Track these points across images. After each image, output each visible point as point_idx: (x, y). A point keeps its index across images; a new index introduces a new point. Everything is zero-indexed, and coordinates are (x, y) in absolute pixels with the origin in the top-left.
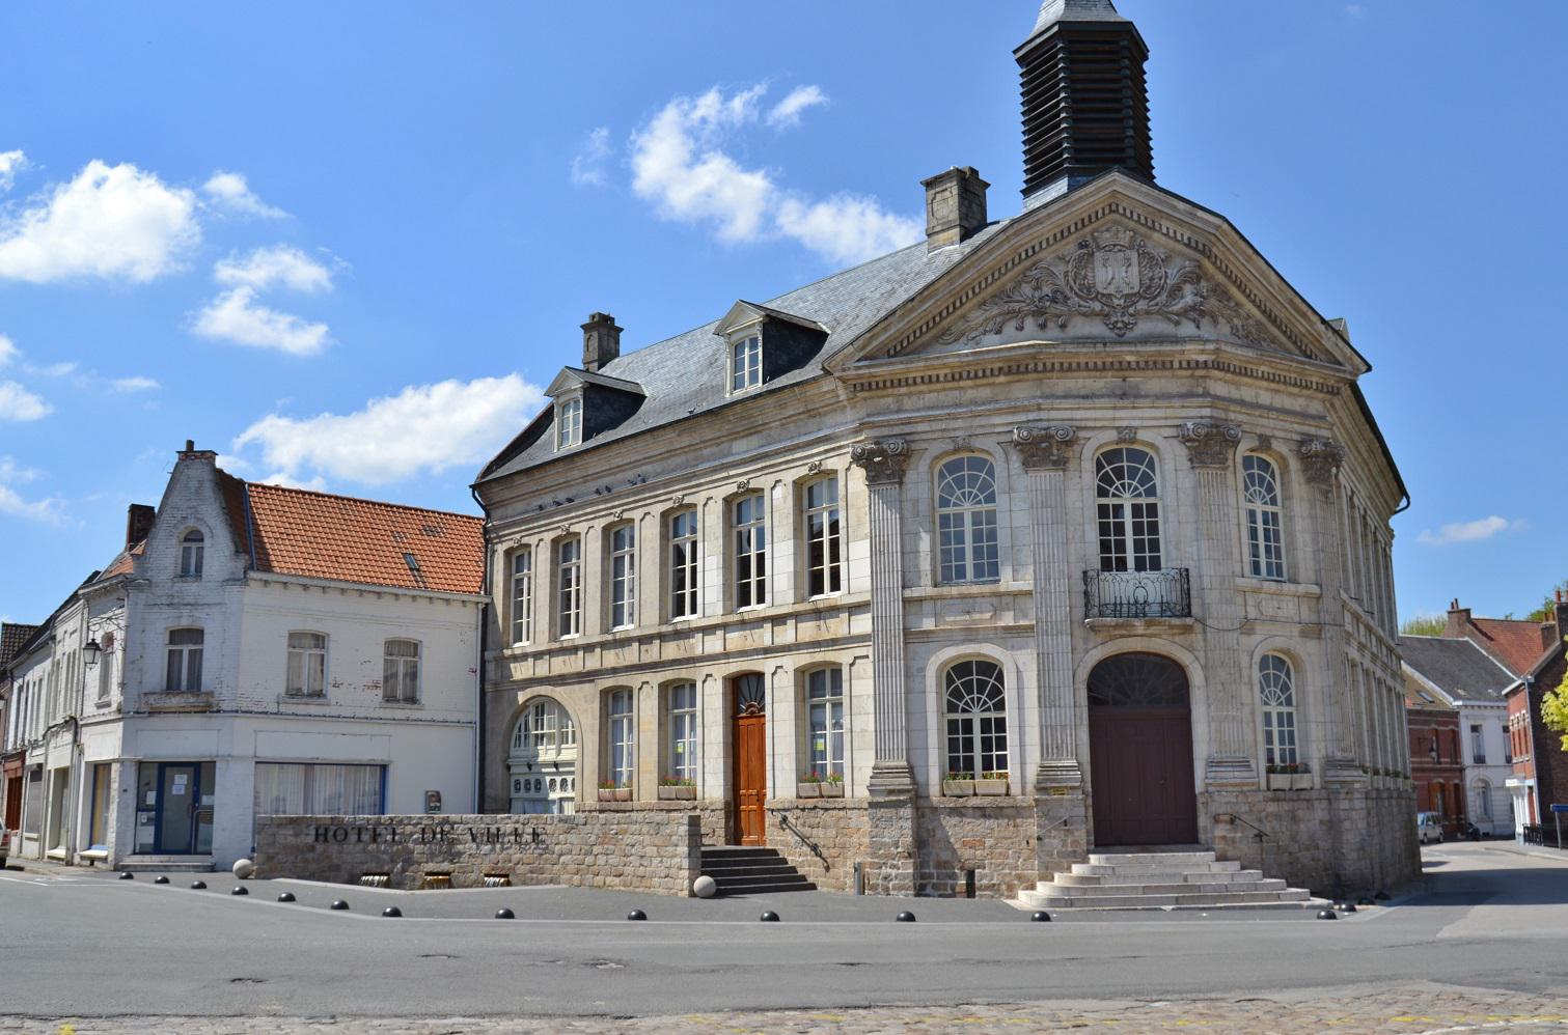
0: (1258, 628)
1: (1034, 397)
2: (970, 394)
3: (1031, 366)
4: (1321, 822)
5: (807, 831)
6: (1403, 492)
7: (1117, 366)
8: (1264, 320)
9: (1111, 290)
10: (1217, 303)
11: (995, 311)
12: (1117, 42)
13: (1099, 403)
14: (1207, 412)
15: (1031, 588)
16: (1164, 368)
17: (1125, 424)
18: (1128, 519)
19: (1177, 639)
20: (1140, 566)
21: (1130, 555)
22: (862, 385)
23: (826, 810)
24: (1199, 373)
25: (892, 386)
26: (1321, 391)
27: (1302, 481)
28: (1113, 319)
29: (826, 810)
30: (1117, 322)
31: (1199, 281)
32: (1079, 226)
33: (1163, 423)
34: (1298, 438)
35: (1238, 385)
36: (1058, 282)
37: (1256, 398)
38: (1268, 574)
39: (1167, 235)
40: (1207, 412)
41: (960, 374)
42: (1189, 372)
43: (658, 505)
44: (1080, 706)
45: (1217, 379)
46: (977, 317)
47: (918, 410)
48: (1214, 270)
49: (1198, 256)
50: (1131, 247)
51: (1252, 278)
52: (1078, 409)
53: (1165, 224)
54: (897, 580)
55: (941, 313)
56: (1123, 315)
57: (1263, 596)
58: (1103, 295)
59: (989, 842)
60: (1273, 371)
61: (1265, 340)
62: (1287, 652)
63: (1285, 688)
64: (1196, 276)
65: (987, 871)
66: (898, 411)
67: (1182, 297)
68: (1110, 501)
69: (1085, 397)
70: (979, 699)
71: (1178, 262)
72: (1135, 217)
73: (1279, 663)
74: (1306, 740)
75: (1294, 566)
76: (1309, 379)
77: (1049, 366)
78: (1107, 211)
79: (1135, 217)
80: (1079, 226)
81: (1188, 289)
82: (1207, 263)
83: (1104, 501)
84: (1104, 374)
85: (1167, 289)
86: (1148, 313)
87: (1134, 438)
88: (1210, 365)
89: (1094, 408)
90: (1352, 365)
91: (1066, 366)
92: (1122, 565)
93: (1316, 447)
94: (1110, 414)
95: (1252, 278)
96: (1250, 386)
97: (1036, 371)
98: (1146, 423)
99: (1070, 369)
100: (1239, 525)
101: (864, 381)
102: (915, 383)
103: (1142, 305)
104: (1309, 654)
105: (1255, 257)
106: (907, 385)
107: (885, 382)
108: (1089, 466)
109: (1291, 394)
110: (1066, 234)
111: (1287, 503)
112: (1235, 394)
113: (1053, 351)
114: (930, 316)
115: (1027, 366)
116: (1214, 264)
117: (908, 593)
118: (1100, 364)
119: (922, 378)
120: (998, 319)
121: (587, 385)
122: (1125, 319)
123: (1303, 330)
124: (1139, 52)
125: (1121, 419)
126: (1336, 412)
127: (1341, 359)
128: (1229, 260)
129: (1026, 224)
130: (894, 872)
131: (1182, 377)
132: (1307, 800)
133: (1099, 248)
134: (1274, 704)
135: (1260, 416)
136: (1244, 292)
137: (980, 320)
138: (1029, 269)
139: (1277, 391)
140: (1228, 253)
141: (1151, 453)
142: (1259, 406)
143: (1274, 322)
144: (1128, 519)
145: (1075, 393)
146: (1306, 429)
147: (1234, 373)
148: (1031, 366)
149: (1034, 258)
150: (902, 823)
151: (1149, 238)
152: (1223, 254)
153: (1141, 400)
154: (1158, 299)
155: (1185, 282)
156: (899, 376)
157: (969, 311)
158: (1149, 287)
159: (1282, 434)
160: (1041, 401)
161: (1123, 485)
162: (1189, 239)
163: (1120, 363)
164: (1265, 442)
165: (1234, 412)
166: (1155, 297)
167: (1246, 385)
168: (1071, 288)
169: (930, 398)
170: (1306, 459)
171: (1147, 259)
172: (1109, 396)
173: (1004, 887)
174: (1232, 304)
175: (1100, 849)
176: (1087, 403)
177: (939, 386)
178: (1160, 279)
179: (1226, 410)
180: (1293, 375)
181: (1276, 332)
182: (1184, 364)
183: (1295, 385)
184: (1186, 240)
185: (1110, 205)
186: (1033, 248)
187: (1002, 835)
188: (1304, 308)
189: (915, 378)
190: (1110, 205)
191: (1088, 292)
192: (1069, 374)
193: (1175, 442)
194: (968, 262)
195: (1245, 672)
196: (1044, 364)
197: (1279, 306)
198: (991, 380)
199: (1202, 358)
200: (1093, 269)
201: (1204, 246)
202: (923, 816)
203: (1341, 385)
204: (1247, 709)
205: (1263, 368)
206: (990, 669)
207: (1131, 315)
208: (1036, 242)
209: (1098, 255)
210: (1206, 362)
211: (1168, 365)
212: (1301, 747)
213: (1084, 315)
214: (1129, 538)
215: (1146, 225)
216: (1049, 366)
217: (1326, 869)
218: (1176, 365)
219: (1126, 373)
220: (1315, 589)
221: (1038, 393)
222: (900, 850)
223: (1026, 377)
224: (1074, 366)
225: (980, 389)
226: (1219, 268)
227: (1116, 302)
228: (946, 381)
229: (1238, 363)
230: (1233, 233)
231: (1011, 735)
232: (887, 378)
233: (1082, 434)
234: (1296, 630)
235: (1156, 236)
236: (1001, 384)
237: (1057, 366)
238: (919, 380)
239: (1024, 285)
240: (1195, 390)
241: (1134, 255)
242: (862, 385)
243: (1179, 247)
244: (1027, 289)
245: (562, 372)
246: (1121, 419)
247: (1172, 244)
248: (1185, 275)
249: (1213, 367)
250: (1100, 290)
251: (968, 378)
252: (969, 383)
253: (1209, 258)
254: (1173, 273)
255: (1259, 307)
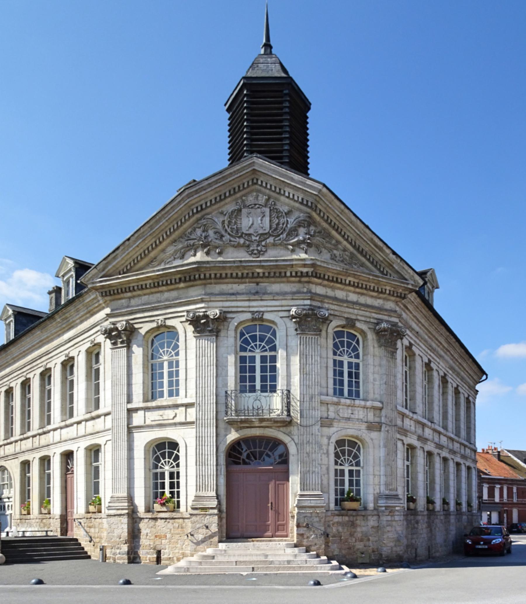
0: (335, 424)
1: (200, 295)
2: (166, 295)
3: (197, 276)
4: (373, 527)
5: (88, 529)
6: (483, 373)
7: (250, 275)
8: (355, 252)
9: (251, 231)
10: (321, 240)
11: (180, 246)
12: (282, 91)
13: (239, 297)
14: (308, 302)
15: (194, 401)
16: (280, 276)
17: (255, 309)
18: (258, 364)
19: (281, 429)
20: (264, 389)
21: (258, 384)
22: (106, 292)
23: (95, 519)
24: (304, 279)
25: (122, 292)
26: (393, 295)
27: (376, 345)
28: (251, 248)
29: (95, 519)
30: (253, 250)
31: (309, 226)
32: (232, 192)
33: (280, 308)
34: (375, 321)
35: (333, 288)
36: (218, 227)
37: (346, 297)
38: (349, 396)
39: (288, 197)
40: (308, 302)
41: (158, 283)
42: (298, 279)
43: (39, 369)
44: (221, 465)
45: (317, 284)
46: (171, 250)
47: (138, 306)
48: (325, 221)
49: (309, 210)
50: (266, 206)
51: (346, 225)
52: (227, 301)
53: (287, 190)
54: (125, 398)
55: (148, 248)
56: (258, 245)
57: (340, 407)
58: (246, 234)
59: (168, 536)
60: (356, 281)
61: (355, 264)
62: (357, 438)
63: (356, 457)
64: (309, 222)
65: (167, 551)
66: (128, 307)
67: (297, 235)
68: (248, 354)
69: (233, 294)
70: (169, 462)
71: (296, 214)
72: (269, 187)
73: (353, 444)
74: (366, 485)
75: (366, 392)
76: (384, 287)
77: (208, 276)
78: (250, 183)
79: (269, 187)
80: (232, 192)
81: (302, 231)
82: (314, 214)
83: (243, 354)
84: (243, 280)
85: (287, 230)
86: (274, 245)
87: (262, 317)
88: (310, 274)
89: (236, 300)
90: (415, 281)
91: (218, 275)
92: (253, 389)
93: (384, 325)
94: (247, 304)
95: (346, 225)
96: (342, 290)
97: (200, 279)
98: (269, 309)
99: (221, 277)
100: (327, 367)
101: (106, 290)
102: (134, 290)
103: (271, 240)
104: (372, 439)
105: (346, 211)
106: (130, 291)
107: (118, 290)
108: (231, 333)
109: (372, 297)
110: (223, 197)
111: (365, 357)
112: (330, 293)
113: (208, 265)
114: (142, 251)
115: (195, 276)
116: (319, 215)
117: (130, 406)
118: (240, 274)
119: (138, 286)
120: (182, 251)
121: (16, 313)
122: (259, 248)
123: (381, 259)
124: (301, 105)
125: (253, 307)
126: (411, 313)
127: (406, 277)
128: (329, 213)
129: (194, 189)
130: (118, 551)
131: (294, 282)
132: (364, 516)
133: (245, 206)
134: (347, 465)
135: (347, 307)
136: (340, 233)
137: (172, 252)
138: (200, 219)
139: (362, 294)
140: (328, 208)
141: (274, 326)
142: (347, 301)
143: (361, 253)
144: (258, 364)
145: (226, 292)
146: (380, 316)
147: (328, 280)
148: (197, 276)
149: (203, 213)
150: (123, 526)
151: (279, 200)
152: (325, 209)
153: (266, 296)
154: (281, 236)
155: (299, 226)
156: (125, 286)
157: (167, 247)
158: (276, 229)
159: (363, 319)
160: (204, 297)
161: (256, 345)
162: (302, 199)
163: (253, 273)
164: (351, 323)
165: (328, 303)
166: (279, 235)
167: (339, 289)
168: (226, 231)
169: (145, 299)
170: (379, 333)
171: (274, 210)
172: (247, 294)
173: (175, 558)
174: (334, 242)
175: (229, 540)
176: (233, 298)
177: (148, 291)
178: (283, 224)
179: (321, 302)
180: (373, 285)
181: (363, 259)
182: (294, 274)
183: (374, 290)
184: (300, 200)
185: (253, 180)
186: (201, 206)
187: (176, 532)
188: (380, 244)
189: (133, 287)
190: (253, 180)
191: (238, 233)
192: (221, 281)
193: (287, 320)
194: (160, 215)
195: (325, 447)
196: (205, 275)
197: (364, 243)
198: (177, 286)
199: (305, 270)
200: (241, 219)
201: (312, 203)
202: (136, 522)
203: (407, 292)
204: (324, 468)
205: (349, 279)
206: (174, 445)
207: (263, 246)
208: (203, 202)
209: (244, 211)
210: (307, 273)
211: (283, 274)
212: (363, 488)
213: (233, 246)
214: (258, 374)
215: (275, 191)
216: (208, 276)
217: (373, 551)
218: (288, 274)
219: (258, 280)
220: (379, 405)
221: (203, 293)
222: (121, 540)
223: (195, 283)
224: (224, 275)
225: (172, 292)
226: (323, 218)
227: (254, 238)
228: (151, 288)
229: (331, 275)
230: (330, 195)
231: (182, 480)
232: (119, 287)
233: (229, 315)
234: (364, 426)
235: (282, 198)
236: (182, 288)
237: (213, 276)
238: (136, 288)
239: (197, 229)
240: (302, 290)
241: (267, 210)
242: (106, 292)
243: (297, 205)
244: (199, 232)
245: (5, 308)
246: (253, 307)
247: (292, 203)
248: (299, 222)
249: (312, 276)
250: (245, 232)
251: (163, 285)
252: (164, 288)
253: (315, 211)
254: (292, 221)
255: (351, 243)
